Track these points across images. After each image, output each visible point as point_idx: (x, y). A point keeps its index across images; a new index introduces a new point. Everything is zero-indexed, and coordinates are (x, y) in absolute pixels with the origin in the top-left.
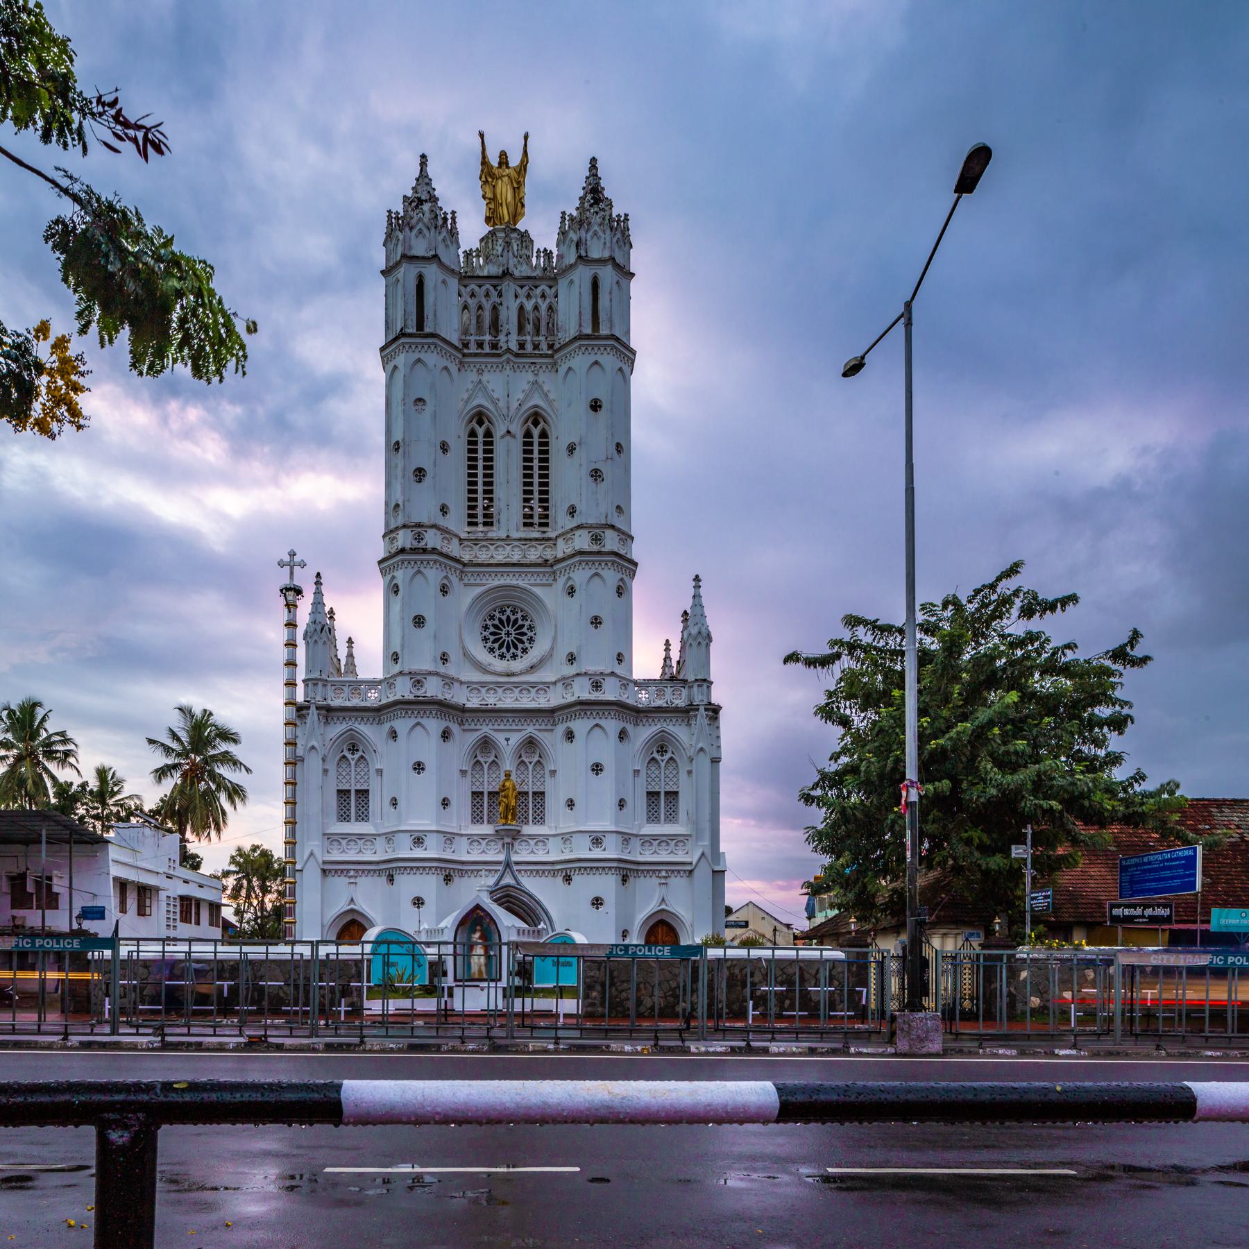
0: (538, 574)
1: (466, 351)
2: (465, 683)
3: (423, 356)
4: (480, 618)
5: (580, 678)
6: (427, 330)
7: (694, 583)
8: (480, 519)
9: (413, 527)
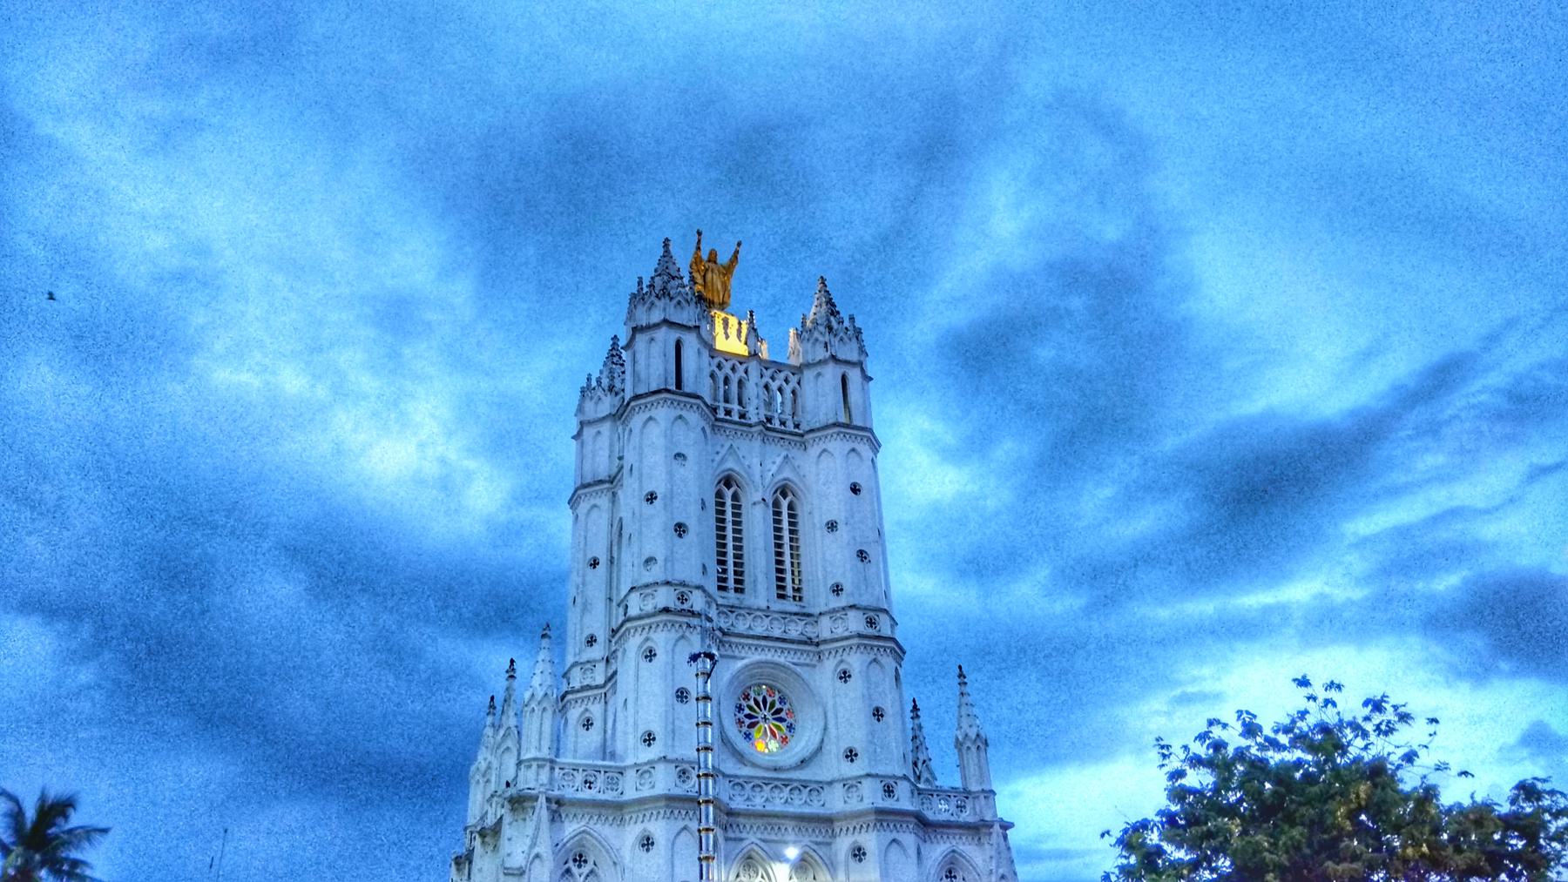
0: (808, 653)
1: (769, 425)
2: (728, 776)
3: (684, 413)
4: (736, 697)
5: (870, 779)
6: (687, 388)
7: (959, 680)
8: (790, 592)
9: (676, 585)
